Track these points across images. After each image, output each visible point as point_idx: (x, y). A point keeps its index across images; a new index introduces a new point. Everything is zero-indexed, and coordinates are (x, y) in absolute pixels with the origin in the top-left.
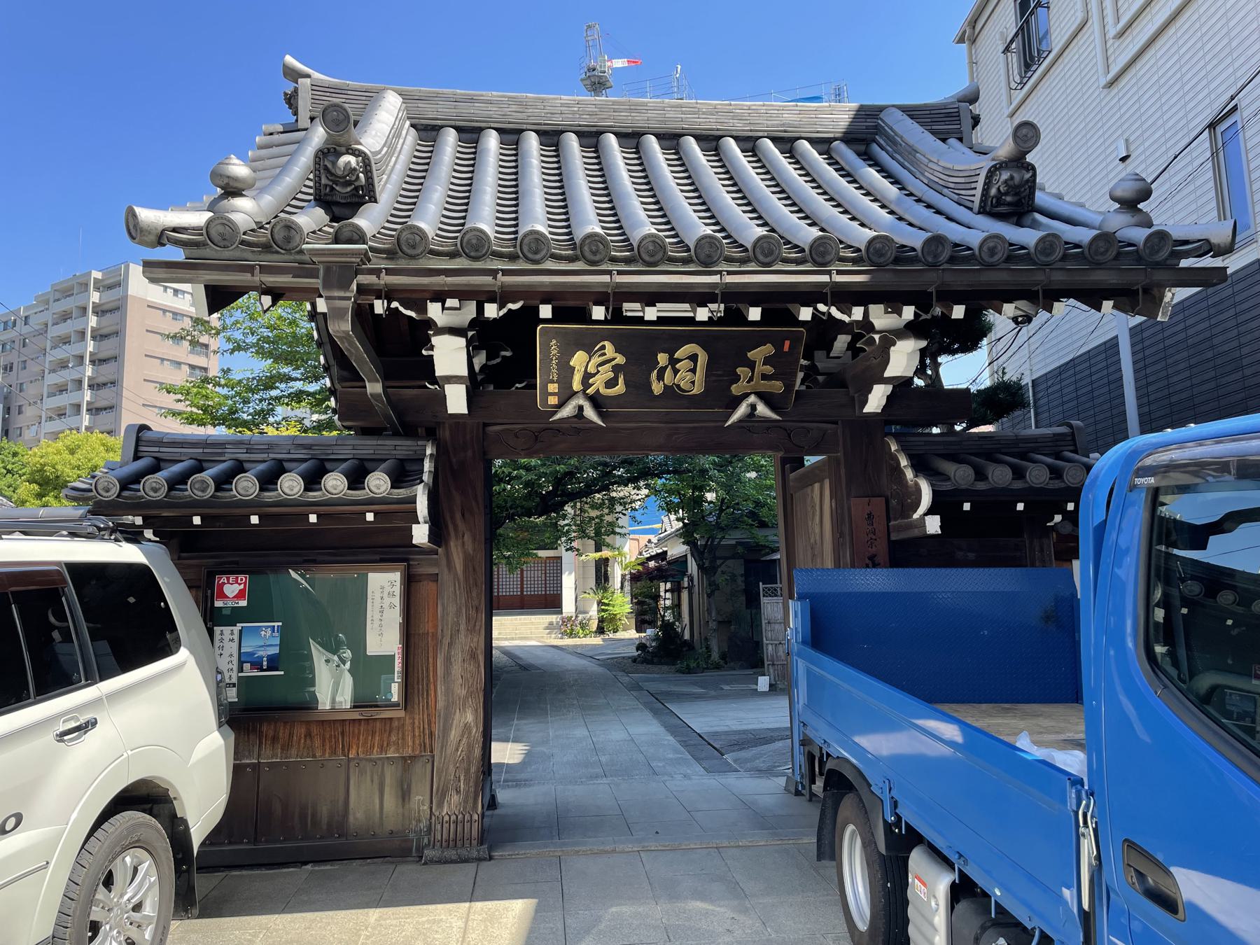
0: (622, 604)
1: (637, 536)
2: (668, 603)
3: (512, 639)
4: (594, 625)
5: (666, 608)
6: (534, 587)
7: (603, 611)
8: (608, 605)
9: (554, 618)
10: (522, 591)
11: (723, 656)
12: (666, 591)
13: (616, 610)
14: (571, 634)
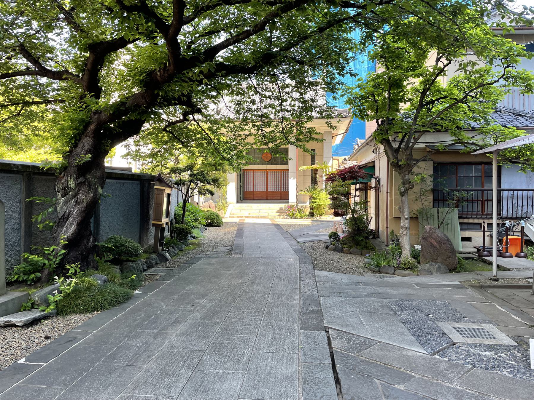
0: (325, 199)
1: (337, 157)
2: (358, 199)
3: (256, 217)
4: (308, 211)
5: (356, 204)
6: (274, 187)
7: (313, 202)
8: (316, 199)
9: (283, 206)
10: (267, 189)
11: (415, 255)
12: (356, 190)
13: (322, 202)
14: (293, 216)
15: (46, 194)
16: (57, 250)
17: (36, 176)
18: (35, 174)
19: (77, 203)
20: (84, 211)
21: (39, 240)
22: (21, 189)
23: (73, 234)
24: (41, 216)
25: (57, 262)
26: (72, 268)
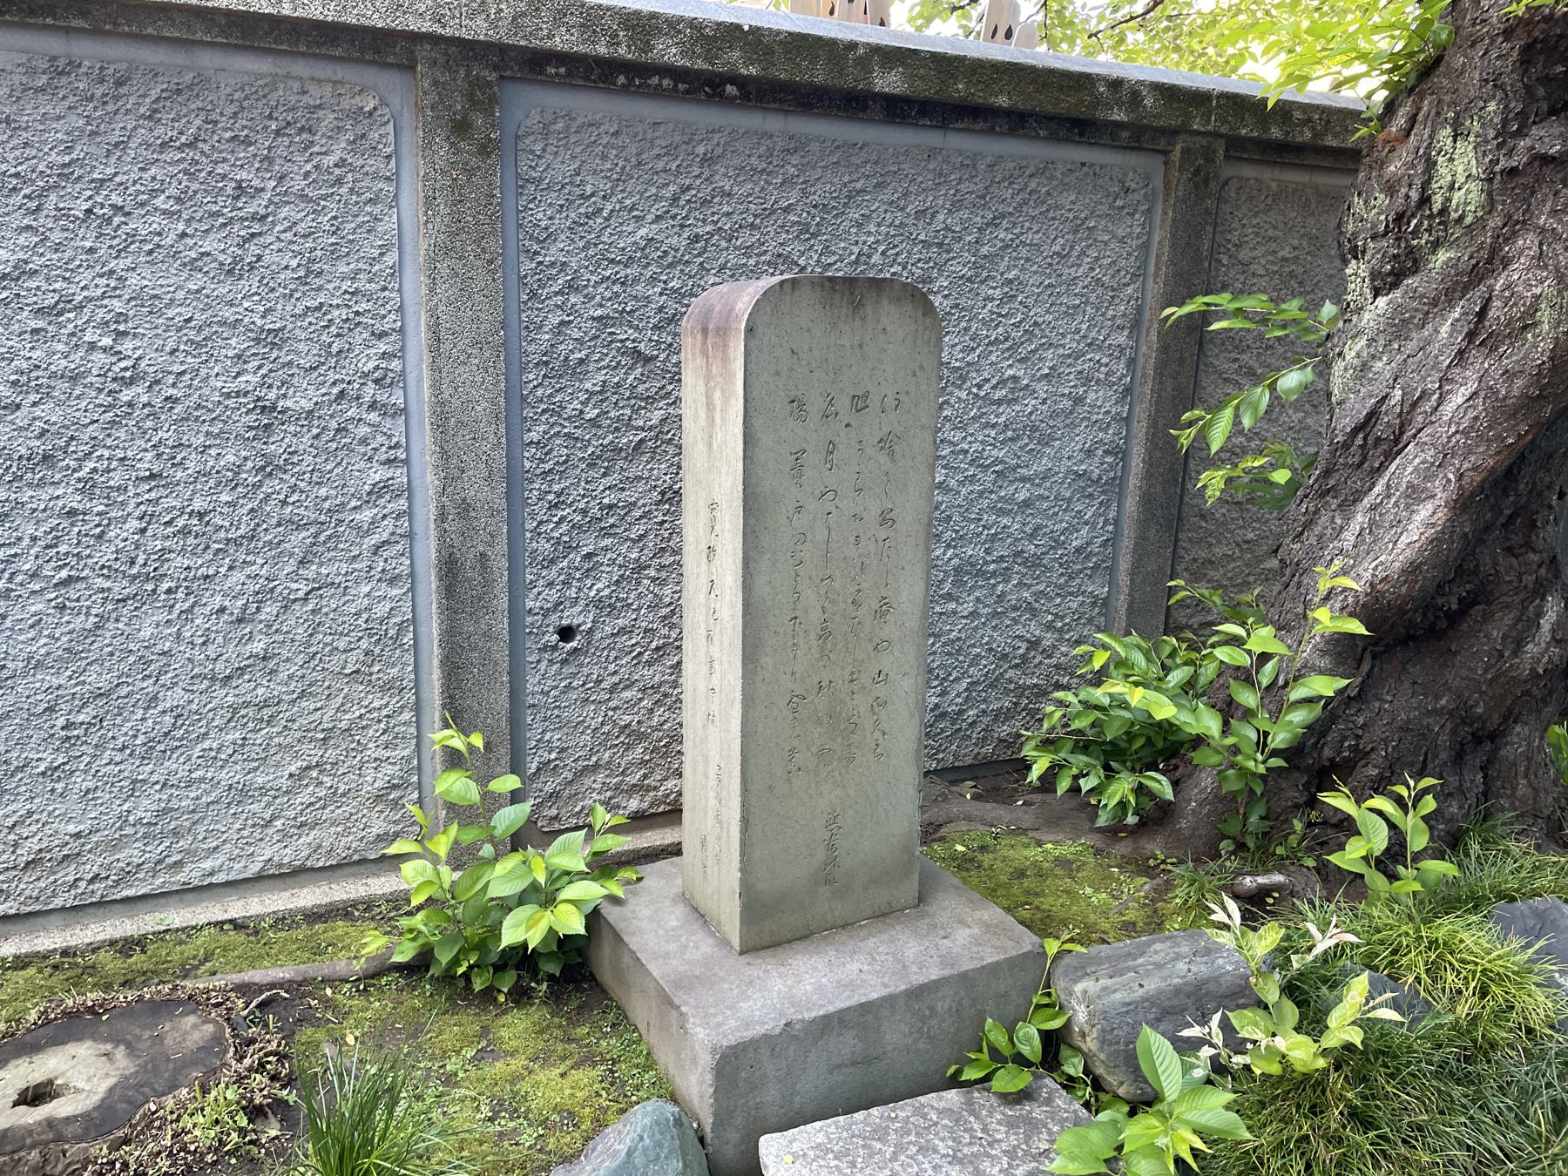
15: (1287, 282)
16: (1287, 659)
17: (1248, 171)
18: (1237, 148)
19: (1478, 335)
20: (1528, 402)
21: (1219, 551)
22: (1145, 247)
23: (1412, 569)
24: (1228, 413)
25: (1279, 739)
26: (1372, 819)
